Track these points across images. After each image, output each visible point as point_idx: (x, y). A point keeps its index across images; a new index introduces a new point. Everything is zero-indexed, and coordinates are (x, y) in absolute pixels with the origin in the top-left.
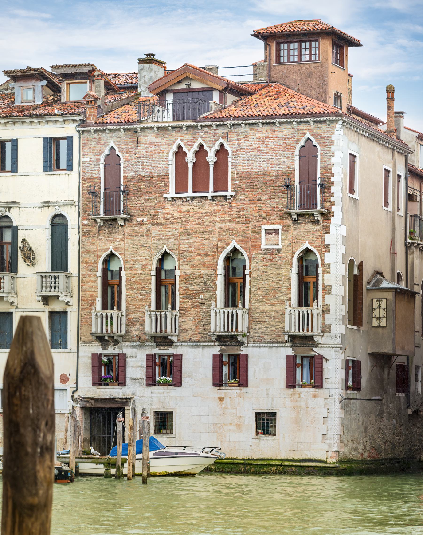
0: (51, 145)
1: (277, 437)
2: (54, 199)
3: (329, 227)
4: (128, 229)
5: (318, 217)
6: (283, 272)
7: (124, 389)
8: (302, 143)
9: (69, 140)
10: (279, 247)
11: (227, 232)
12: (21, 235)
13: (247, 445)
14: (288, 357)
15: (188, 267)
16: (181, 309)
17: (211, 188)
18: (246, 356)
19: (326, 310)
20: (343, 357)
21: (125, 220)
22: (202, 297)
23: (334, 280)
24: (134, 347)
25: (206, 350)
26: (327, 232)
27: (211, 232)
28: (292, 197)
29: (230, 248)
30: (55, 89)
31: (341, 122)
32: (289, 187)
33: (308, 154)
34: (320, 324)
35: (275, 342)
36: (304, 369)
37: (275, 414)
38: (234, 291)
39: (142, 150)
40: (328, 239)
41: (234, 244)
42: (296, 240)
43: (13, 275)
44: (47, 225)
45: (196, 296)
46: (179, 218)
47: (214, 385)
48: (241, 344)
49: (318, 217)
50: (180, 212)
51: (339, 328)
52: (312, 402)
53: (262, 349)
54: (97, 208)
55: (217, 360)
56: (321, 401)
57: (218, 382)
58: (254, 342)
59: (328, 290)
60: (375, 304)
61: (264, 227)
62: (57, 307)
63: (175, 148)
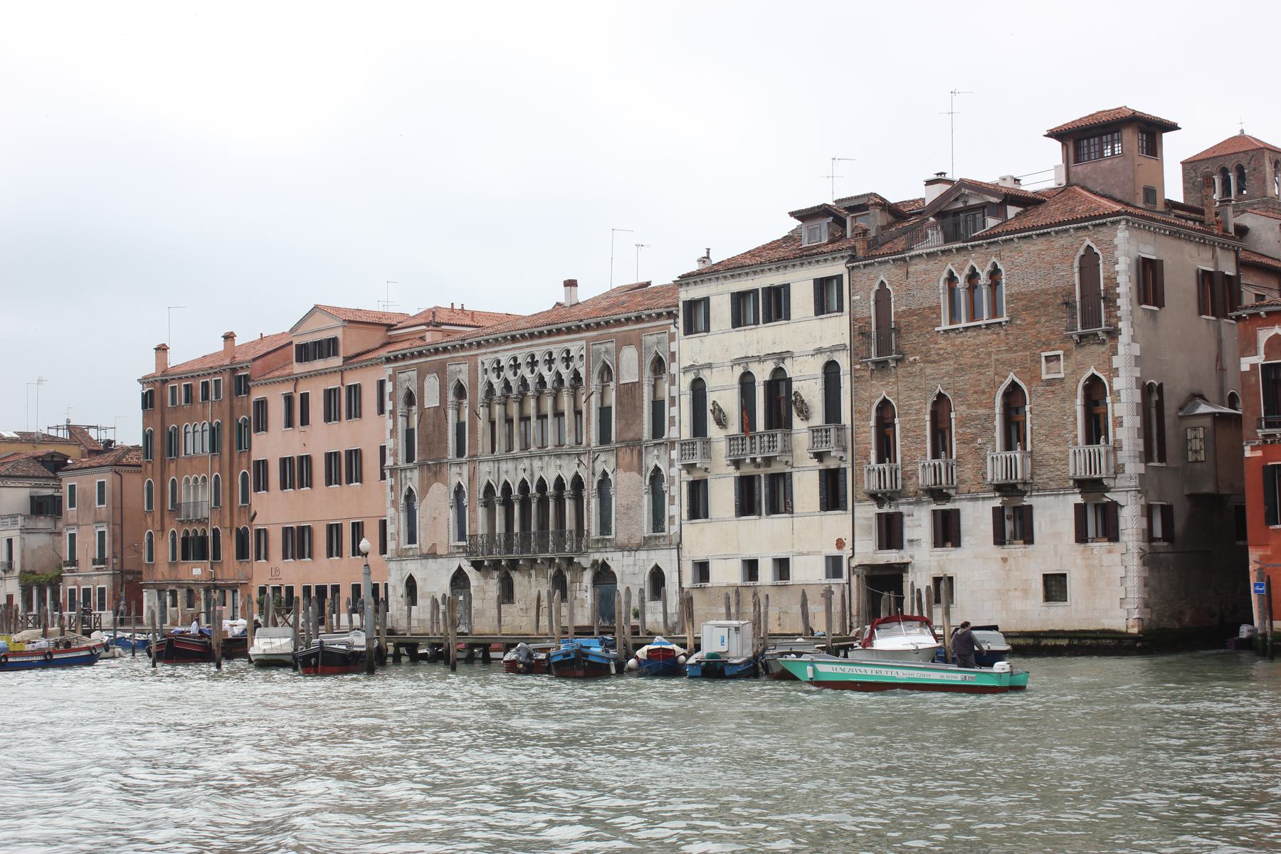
0: (822, 286)
1: (1068, 603)
2: (826, 345)
3: (1116, 348)
4: (901, 371)
5: (1102, 336)
6: (1067, 405)
7: (902, 552)
8: (1081, 252)
9: (839, 278)
10: (1062, 375)
11: (1003, 363)
12: (795, 386)
13: (1038, 615)
14: (1076, 505)
15: (963, 408)
16: (958, 457)
17: (985, 316)
18: (1030, 507)
19: (1117, 448)
20: (1143, 501)
21: (897, 360)
22: (979, 441)
23: (1123, 409)
24: (910, 504)
25: (987, 502)
26: (1115, 353)
27: (987, 365)
28: (1073, 316)
29: (1007, 382)
30: (840, 222)
31: (1123, 222)
32: (1069, 305)
33: (1089, 263)
34: (1112, 464)
35: (1059, 491)
36: (1097, 521)
37: (1064, 576)
38: (1014, 433)
39: (912, 280)
40: (1117, 362)
41: (1012, 377)
42: (1081, 367)
43: (786, 431)
44: (819, 371)
45: (974, 440)
46: (953, 352)
47: (995, 543)
48: (1024, 493)
49: (1102, 336)
50: (954, 345)
51: (1133, 468)
52: (1107, 559)
53: (1047, 498)
54: (869, 349)
55: (998, 514)
56: (1116, 557)
57: (999, 539)
58: (1038, 490)
59: (1119, 422)
60: (1190, 435)
61: (1044, 354)
62: (832, 464)
63: (945, 275)
